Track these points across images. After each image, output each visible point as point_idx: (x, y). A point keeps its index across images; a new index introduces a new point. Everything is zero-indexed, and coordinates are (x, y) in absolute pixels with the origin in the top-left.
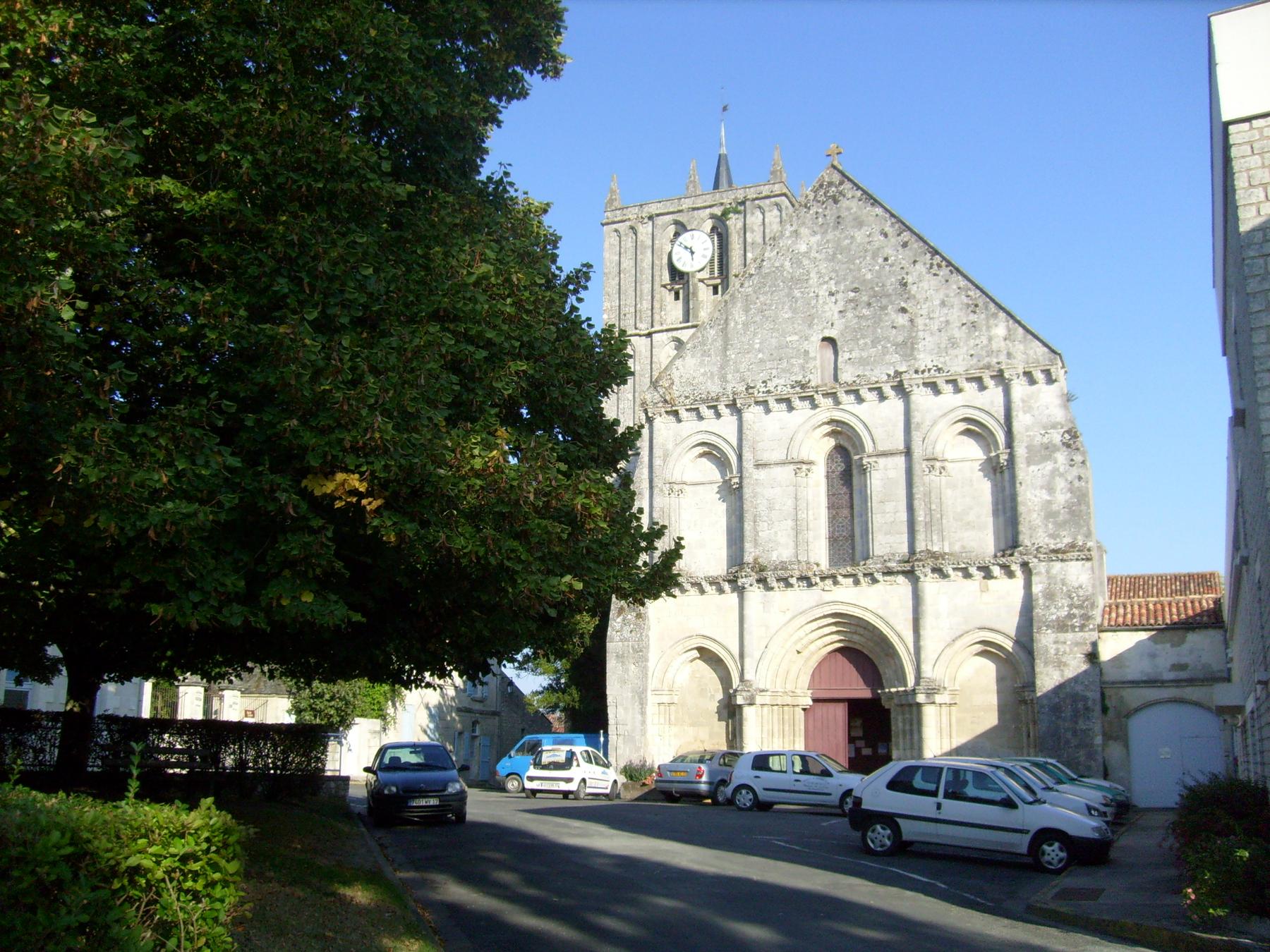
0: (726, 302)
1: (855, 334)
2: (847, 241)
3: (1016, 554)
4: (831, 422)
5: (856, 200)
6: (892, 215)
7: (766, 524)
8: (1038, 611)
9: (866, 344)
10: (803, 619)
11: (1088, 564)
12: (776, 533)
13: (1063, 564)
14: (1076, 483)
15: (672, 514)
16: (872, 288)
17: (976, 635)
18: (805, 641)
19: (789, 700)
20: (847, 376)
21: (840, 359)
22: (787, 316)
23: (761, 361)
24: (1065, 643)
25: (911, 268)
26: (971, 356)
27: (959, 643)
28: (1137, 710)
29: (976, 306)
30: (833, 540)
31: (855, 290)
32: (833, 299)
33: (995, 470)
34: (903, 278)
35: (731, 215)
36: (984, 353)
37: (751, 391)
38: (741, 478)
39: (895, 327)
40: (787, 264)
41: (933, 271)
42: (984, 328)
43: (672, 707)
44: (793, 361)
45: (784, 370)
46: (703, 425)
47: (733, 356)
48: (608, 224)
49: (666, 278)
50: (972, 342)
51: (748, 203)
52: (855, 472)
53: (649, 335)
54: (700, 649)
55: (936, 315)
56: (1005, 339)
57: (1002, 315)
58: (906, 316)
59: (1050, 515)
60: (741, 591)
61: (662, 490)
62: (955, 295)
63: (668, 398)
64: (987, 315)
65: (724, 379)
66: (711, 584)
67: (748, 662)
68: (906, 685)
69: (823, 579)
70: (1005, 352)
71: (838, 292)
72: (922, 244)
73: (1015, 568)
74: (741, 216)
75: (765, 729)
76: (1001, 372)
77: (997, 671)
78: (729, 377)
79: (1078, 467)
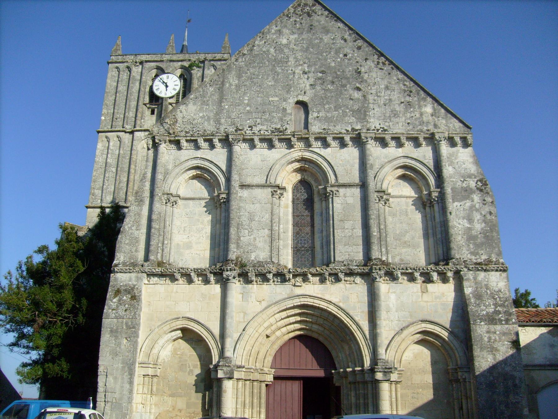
0: (223, 70)
1: (322, 101)
2: (317, 41)
3: (450, 264)
4: (302, 160)
5: (324, 17)
6: (350, 28)
7: (246, 231)
8: (472, 308)
9: (330, 108)
10: (276, 309)
11: (504, 275)
12: (255, 239)
13: (486, 273)
14: (489, 217)
15: (167, 219)
16: (336, 73)
17: (419, 326)
18: (273, 328)
19: (257, 376)
20: (316, 128)
21: (310, 117)
23: (248, 112)
24: (495, 333)
25: (364, 63)
26: (408, 123)
27: (406, 332)
28: (544, 387)
29: (411, 92)
30: (296, 250)
31: (323, 72)
32: (306, 76)
33: (424, 206)
34: (358, 69)
35: (195, 68)
36: (417, 123)
38: (228, 194)
39: (352, 99)
40: (272, 50)
41: (379, 66)
42: (417, 107)
43: (155, 380)
44: (274, 114)
45: (266, 120)
46: (199, 154)
47: (227, 107)
48: (112, 63)
49: (147, 100)
50: (408, 115)
51: (206, 62)
52: (316, 199)
53: (132, 133)
54: (184, 330)
55: (383, 94)
56: (432, 115)
57: (429, 99)
58: (360, 93)
59: (470, 238)
60: (224, 283)
61: (161, 199)
62: (396, 83)
63: (171, 132)
64: (418, 99)
66: (198, 275)
67: (229, 343)
68: (363, 366)
69: (295, 276)
70: (432, 123)
71: (309, 72)
72: (371, 49)
73: (450, 274)
74: (201, 70)
75: (240, 400)
76: (433, 134)
77: (432, 355)
78: (223, 121)
79: (489, 206)
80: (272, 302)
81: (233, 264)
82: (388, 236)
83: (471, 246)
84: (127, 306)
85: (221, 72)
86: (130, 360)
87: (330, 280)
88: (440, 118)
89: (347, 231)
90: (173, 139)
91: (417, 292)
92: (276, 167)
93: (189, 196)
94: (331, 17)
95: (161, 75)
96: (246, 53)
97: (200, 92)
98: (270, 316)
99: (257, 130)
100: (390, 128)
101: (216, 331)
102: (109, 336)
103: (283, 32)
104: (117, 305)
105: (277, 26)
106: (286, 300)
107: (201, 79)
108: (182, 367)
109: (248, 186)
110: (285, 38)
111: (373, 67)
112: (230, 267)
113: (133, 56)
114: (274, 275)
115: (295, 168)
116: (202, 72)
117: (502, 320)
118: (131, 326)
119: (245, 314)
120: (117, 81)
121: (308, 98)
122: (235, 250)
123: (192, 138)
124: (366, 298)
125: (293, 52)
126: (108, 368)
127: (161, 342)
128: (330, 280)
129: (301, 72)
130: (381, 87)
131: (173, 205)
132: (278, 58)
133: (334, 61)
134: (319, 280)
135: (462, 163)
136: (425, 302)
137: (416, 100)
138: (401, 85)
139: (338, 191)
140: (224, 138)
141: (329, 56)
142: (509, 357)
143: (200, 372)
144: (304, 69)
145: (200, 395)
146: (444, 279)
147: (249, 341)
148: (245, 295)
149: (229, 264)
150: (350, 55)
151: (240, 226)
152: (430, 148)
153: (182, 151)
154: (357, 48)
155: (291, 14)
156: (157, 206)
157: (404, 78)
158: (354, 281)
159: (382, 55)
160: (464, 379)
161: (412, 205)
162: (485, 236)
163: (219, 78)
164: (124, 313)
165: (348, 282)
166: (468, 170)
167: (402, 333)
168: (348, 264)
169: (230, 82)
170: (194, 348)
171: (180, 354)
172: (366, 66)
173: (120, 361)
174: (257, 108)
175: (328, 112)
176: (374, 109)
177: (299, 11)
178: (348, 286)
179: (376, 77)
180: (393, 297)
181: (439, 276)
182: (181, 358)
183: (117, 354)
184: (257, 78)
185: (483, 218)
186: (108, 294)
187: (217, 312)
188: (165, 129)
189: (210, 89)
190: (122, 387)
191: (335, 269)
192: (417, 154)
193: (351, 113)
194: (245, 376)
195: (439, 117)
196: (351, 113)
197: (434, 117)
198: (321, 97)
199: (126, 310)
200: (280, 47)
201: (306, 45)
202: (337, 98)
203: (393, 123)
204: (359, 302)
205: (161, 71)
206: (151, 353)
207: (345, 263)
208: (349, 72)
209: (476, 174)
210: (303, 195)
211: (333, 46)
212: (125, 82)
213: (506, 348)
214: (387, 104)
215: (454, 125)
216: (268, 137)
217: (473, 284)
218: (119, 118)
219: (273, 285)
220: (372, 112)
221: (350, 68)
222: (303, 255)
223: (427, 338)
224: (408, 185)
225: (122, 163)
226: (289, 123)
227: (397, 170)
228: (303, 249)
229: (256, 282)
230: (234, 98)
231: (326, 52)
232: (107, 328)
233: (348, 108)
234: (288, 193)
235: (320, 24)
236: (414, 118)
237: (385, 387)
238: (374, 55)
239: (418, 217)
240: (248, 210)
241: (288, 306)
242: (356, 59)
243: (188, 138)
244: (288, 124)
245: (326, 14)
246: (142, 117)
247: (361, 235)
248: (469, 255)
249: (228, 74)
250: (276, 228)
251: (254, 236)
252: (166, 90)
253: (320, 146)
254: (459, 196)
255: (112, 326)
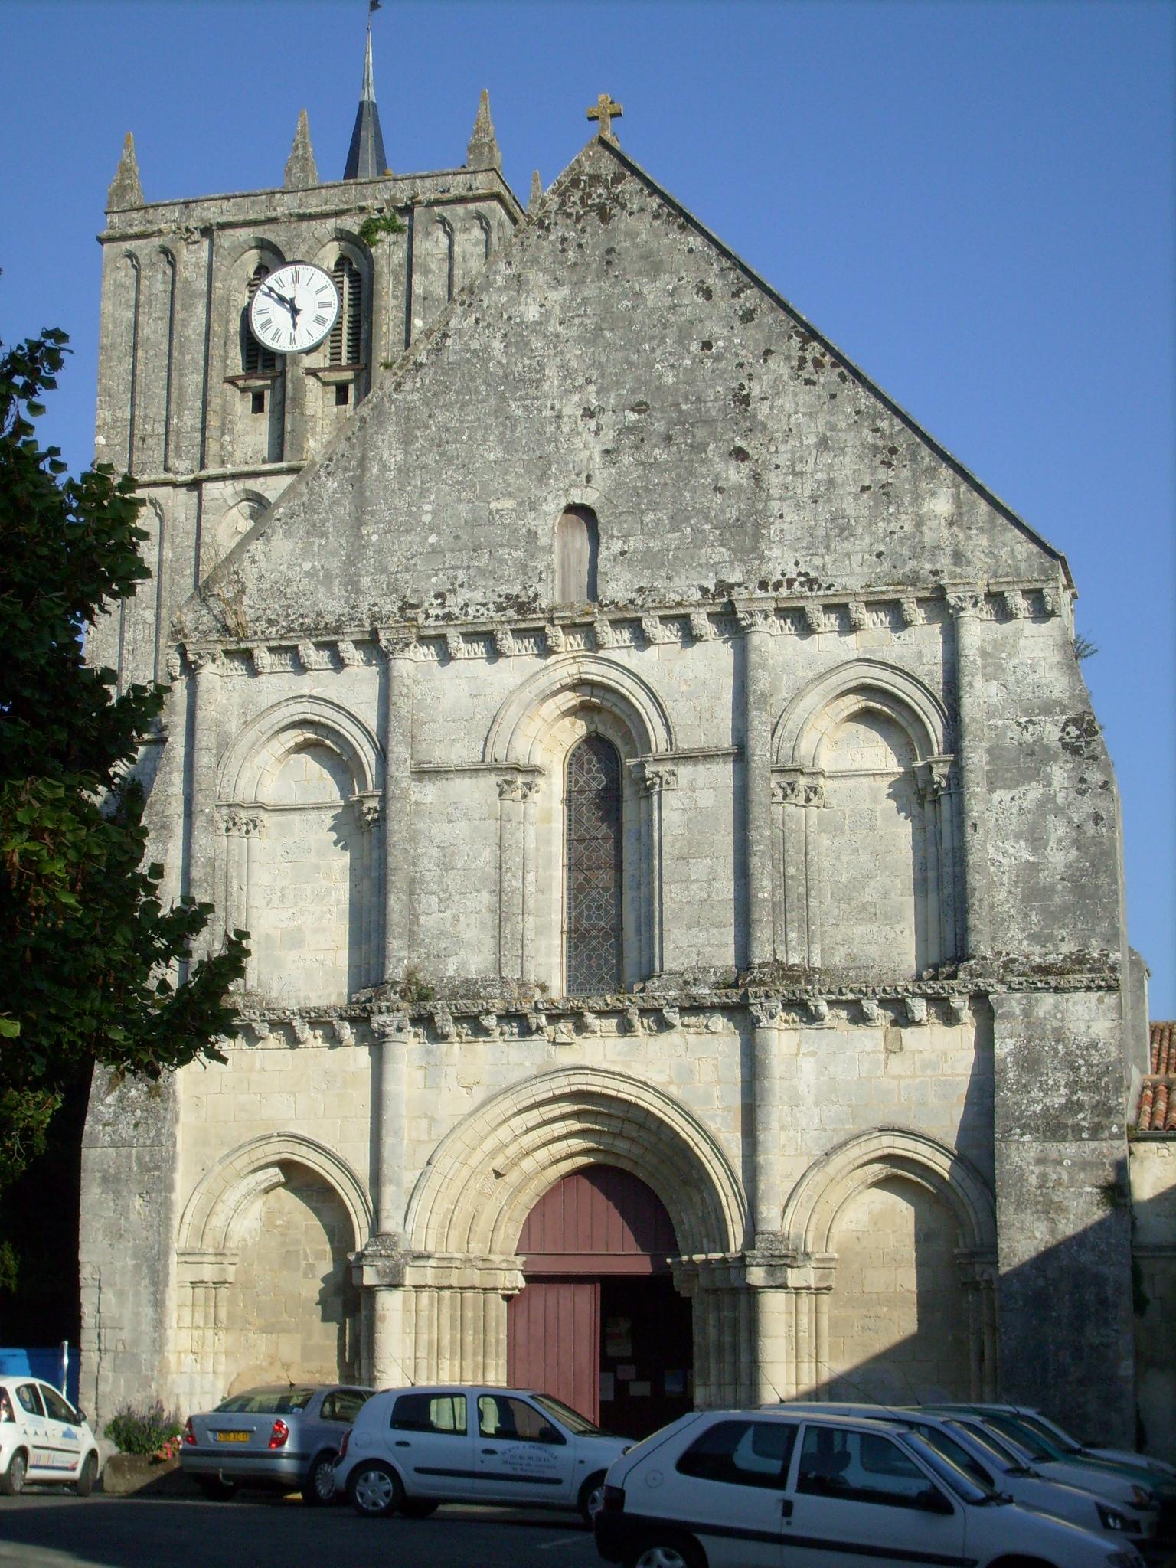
5: (647, 218)
6: (724, 252)
7: (434, 899)
8: (1005, 1096)
9: (658, 522)
10: (508, 1105)
11: (1110, 999)
12: (456, 918)
14: (1090, 829)
17: (875, 1144)
18: (512, 1151)
19: (476, 1278)
20: (616, 588)
21: (603, 553)
22: (492, 456)
23: (435, 550)
24: (1060, 1163)
26: (879, 555)
27: (839, 1161)
29: (893, 451)
30: (577, 937)
31: (640, 408)
34: (742, 387)
35: (381, 235)
36: (906, 552)
37: (410, 613)
38: (384, 799)
39: (721, 490)
40: (497, 345)
41: (804, 374)
42: (907, 499)
43: (223, 1291)
44: (503, 552)
46: (306, 684)
47: (375, 538)
50: (881, 527)
51: (418, 210)
53: (195, 485)
54: (288, 1167)
55: (809, 467)
57: (946, 472)
58: (745, 468)
59: (1032, 891)
60: (376, 1042)
61: (211, 821)
63: (231, 622)
64: (914, 472)
65: (353, 585)
68: (725, 1248)
69: (553, 1018)
70: (949, 550)
71: (602, 410)
72: (782, 315)
74: (403, 239)
75: (424, 1338)
78: (366, 581)
79: (1096, 795)
80: (497, 1089)
81: (395, 993)
82: (813, 893)
83: (1033, 917)
84: (138, 1113)
85: (355, 430)
86: (152, 1248)
87: (646, 1025)
88: (974, 531)
89: (695, 886)
90: (233, 647)
91: (873, 1051)
92: (508, 713)
93: (289, 801)
94: (669, 215)
95: (276, 269)
96: (424, 361)
97: (301, 495)
98: (493, 1125)
99: (456, 605)
100: (827, 574)
101: (362, 1168)
102: (98, 1191)
103: (528, 281)
104: (115, 1113)
105: (510, 263)
106: (534, 1082)
107: (404, 272)
108: (288, 1257)
109: (436, 772)
110: (535, 299)
111: (785, 378)
112: (388, 1004)
113: (177, 209)
114: (500, 1018)
115: (563, 709)
116: (405, 246)
117: (1082, 1129)
118: (151, 1165)
119: (432, 1120)
120: (133, 303)
121: (598, 494)
122: (404, 954)
123: (284, 643)
124: (738, 1072)
125: (555, 347)
126: (102, 1268)
127: (232, 1197)
128: (646, 1025)
129: (580, 412)
130: (805, 442)
131: (248, 832)
132: (513, 372)
133: (672, 366)
134: (618, 1026)
135: (1027, 670)
136: (894, 1077)
137: (906, 479)
138: (866, 431)
139: (674, 775)
140: (367, 637)
141: (658, 352)
142: (1091, 1228)
143: (332, 1269)
144: (588, 401)
145: (334, 1327)
146: (950, 1017)
147: (442, 1190)
148: (430, 1072)
149: (385, 992)
150: (721, 343)
151: (418, 886)
152: (937, 627)
153: (262, 678)
154: (742, 318)
155: (553, 215)
156: (203, 841)
157: (875, 407)
158: (707, 1027)
159: (814, 336)
160: (986, 1281)
161: (889, 796)
162: (1076, 886)
163: (352, 447)
164: (132, 1133)
165: (692, 1030)
166: (1045, 690)
167: (827, 1163)
168: (695, 979)
169: (381, 459)
170: (316, 1211)
171: (281, 1226)
172: (765, 378)
173: (130, 1252)
174: (457, 537)
175: (652, 535)
176: (781, 516)
177: (575, 203)
178: (692, 1039)
179: (792, 411)
180: (808, 1065)
181: (935, 1005)
182: (286, 1235)
183: (121, 1236)
184: (455, 441)
185: (1074, 834)
186: (93, 1085)
187: (363, 1117)
188: (215, 616)
189: (330, 483)
190: (137, 1314)
191: (653, 998)
192: (900, 648)
193: (718, 532)
194: (436, 1277)
195: (970, 528)
196: (718, 532)
197: (955, 528)
198: (635, 488)
199: (136, 1125)
200: (521, 335)
201: (595, 319)
202: (679, 490)
203: (834, 557)
204: (719, 1082)
205: (272, 257)
206: (208, 1227)
207: (686, 976)
208: (716, 399)
209: (1066, 702)
210: (594, 779)
211: (671, 318)
212: (160, 307)
213: (1085, 1202)
214: (820, 496)
215: (1012, 550)
216: (484, 628)
217: (1020, 1029)
218: (151, 436)
219: (500, 1044)
220: (778, 524)
221: (719, 389)
222: (594, 949)
223: (900, 1172)
224: (879, 738)
225: (172, 592)
226: (543, 576)
227: (845, 699)
228: (594, 933)
229: (459, 1035)
230: (396, 509)
231: (653, 338)
232: (93, 1171)
233: (707, 519)
234: (550, 777)
235: (635, 245)
236: (896, 537)
237: (775, 1307)
238: (790, 337)
239: (903, 831)
240: (437, 840)
241: (539, 1098)
242: (737, 355)
243: (274, 644)
244: (540, 579)
245: (655, 205)
246: (224, 424)
247: (732, 897)
248: (1026, 942)
249: (376, 433)
250: (514, 883)
251: (454, 911)
252: (295, 325)
253: (628, 644)
254: (1008, 770)
255: (106, 1166)
